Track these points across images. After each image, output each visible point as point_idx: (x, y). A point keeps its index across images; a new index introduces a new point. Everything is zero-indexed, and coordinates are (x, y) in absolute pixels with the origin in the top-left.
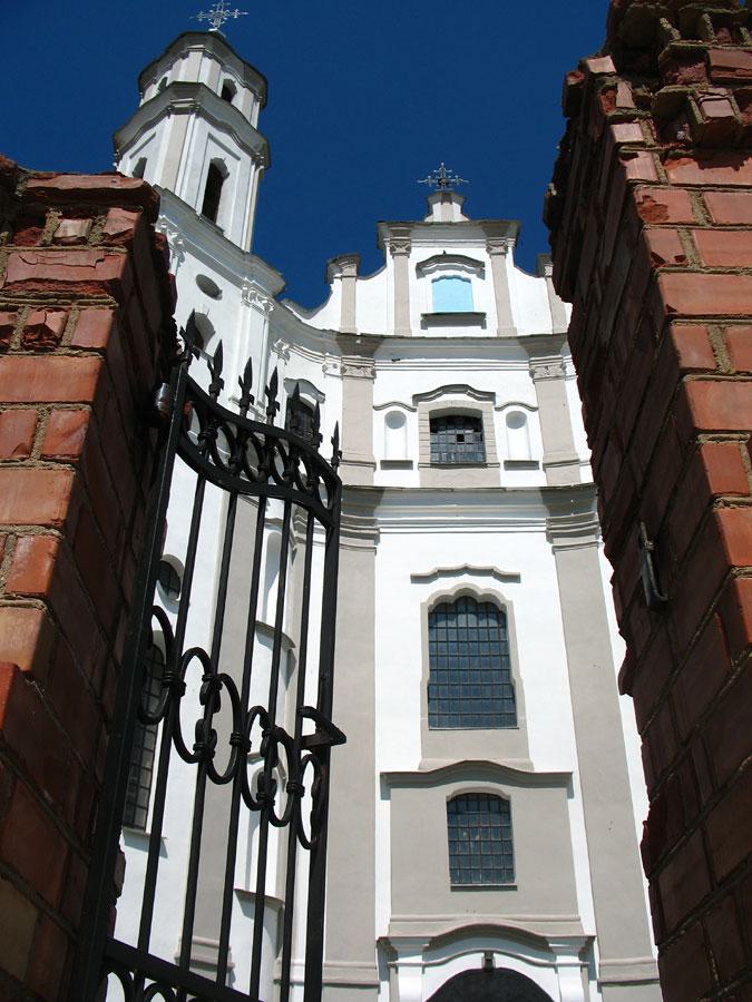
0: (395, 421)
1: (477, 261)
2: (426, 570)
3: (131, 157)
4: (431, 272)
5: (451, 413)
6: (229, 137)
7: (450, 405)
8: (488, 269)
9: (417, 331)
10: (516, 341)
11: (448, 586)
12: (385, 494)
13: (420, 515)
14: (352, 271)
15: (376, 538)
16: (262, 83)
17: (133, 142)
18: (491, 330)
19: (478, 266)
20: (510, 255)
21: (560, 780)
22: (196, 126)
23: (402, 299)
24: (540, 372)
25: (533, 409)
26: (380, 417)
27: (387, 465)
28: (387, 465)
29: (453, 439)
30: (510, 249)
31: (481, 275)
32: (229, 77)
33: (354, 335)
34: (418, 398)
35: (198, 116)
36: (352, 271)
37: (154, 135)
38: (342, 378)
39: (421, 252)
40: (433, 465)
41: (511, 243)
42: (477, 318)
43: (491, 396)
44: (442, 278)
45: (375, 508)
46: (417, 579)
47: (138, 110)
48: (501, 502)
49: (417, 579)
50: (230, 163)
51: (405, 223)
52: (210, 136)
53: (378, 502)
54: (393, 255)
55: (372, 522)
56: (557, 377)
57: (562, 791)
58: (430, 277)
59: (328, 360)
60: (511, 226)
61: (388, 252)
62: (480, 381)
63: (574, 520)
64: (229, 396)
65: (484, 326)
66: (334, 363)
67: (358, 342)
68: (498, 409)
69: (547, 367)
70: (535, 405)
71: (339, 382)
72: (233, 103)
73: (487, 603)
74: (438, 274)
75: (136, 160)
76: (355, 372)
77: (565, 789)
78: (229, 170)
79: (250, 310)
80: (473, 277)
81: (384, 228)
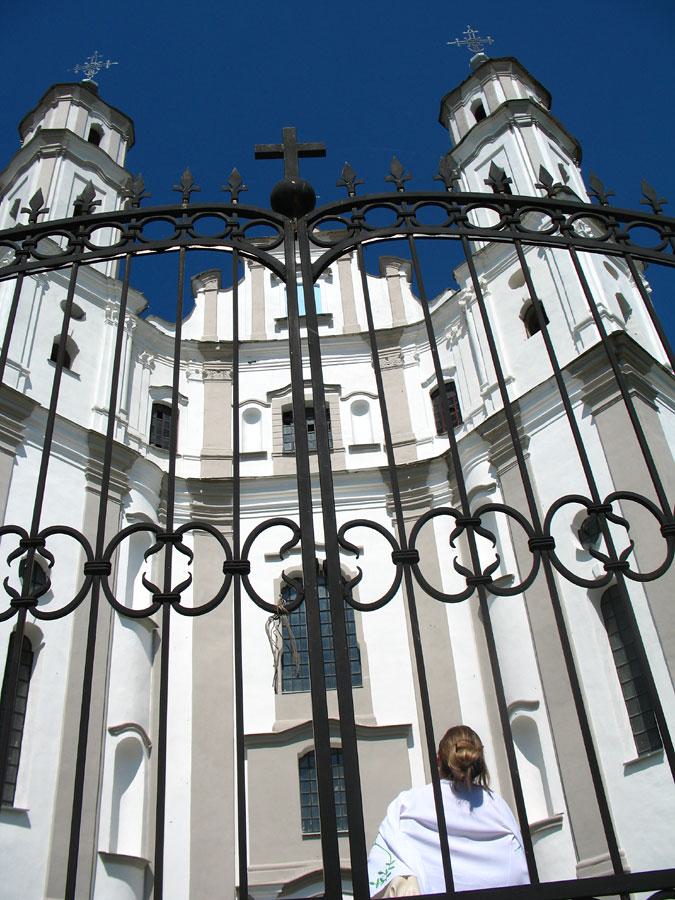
10: (359, 337)
13: (268, 500)
14: (214, 285)
16: (128, 124)
21: (402, 731)
33: (214, 342)
35: (64, 158)
37: (26, 179)
38: (204, 381)
52: (77, 176)
54: (251, 268)
56: (396, 367)
57: (403, 741)
67: (218, 348)
68: (343, 400)
71: (201, 385)
76: (217, 376)
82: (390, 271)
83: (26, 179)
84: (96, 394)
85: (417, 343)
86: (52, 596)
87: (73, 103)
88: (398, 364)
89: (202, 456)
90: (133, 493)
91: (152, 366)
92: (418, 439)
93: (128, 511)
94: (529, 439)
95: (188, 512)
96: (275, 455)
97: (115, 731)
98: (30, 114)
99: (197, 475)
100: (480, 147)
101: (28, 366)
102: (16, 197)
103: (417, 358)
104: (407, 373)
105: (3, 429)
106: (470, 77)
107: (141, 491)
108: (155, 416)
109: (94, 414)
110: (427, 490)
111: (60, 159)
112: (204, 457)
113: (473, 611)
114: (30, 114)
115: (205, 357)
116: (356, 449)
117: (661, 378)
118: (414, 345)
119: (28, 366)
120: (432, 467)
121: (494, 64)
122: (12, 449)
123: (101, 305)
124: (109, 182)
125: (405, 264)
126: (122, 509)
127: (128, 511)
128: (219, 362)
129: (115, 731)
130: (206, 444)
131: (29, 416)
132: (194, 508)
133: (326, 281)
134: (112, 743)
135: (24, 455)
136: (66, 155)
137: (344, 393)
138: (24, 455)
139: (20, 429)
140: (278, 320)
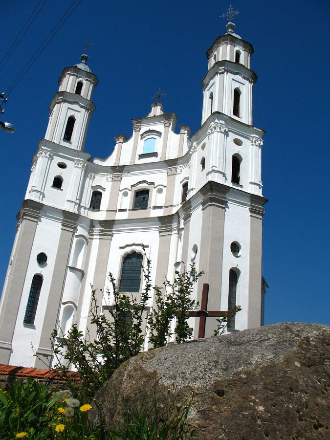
0: (126, 194)
2: (123, 245)
4: (145, 137)
7: (141, 188)
8: (163, 135)
9: (138, 162)
11: (128, 250)
13: (125, 227)
14: (121, 140)
15: (112, 236)
17: (208, 84)
19: (159, 134)
20: (171, 126)
22: (228, 77)
25: (165, 187)
26: (121, 193)
27: (121, 210)
28: (121, 210)
29: (142, 199)
31: (160, 136)
34: (132, 186)
36: (121, 140)
37: (214, 83)
38: (112, 181)
39: (144, 129)
40: (132, 210)
41: (172, 121)
42: (155, 154)
43: (153, 184)
44: (148, 139)
46: (121, 248)
47: (208, 72)
49: (121, 248)
51: (140, 119)
53: (114, 224)
59: (108, 176)
63: (167, 227)
64: (249, 182)
65: (157, 156)
66: (110, 176)
70: (165, 185)
71: (111, 183)
72: (240, 63)
73: (127, 255)
74: (147, 137)
76: (116, 179)
79: (254, 147)
80: (157, 137)
81: (134, 122)
82: (182, 131)
84: (68, 196)
86: (47, 265)
87: (70, 75)
89: (107, 211)
90: (79, 228)
91: (94, 177)
93: (76, 234)
97: (64, 304)
98: (60, 78)
100: (210, 80)
101: (44, 191)
102: (211, 90)
103: (181, 171)
104: (177, 176)
106: (214, 44)
107: (82, 227)
108: (94, 196)
109: (66, 202)
110: (171, 226)
113: (86, 278)
114: (60, 78)
116: (155, 208)
117: (120, 224)
118: (181, 165)
119: (44, 191)
120: (174, 217)
121: (221, 38)
122: (36, 220)
124: (82, 107)
127: (76, 234)
128: (118, 173)
129: (64, 304)
131: (42, 208)
132: (100, 230)
134: (63, 307)
135: (41, 221)
136: (64, 101)
137: (156, 185)
138: (41, 221)
139: (39, 213)
140: (139, 155)
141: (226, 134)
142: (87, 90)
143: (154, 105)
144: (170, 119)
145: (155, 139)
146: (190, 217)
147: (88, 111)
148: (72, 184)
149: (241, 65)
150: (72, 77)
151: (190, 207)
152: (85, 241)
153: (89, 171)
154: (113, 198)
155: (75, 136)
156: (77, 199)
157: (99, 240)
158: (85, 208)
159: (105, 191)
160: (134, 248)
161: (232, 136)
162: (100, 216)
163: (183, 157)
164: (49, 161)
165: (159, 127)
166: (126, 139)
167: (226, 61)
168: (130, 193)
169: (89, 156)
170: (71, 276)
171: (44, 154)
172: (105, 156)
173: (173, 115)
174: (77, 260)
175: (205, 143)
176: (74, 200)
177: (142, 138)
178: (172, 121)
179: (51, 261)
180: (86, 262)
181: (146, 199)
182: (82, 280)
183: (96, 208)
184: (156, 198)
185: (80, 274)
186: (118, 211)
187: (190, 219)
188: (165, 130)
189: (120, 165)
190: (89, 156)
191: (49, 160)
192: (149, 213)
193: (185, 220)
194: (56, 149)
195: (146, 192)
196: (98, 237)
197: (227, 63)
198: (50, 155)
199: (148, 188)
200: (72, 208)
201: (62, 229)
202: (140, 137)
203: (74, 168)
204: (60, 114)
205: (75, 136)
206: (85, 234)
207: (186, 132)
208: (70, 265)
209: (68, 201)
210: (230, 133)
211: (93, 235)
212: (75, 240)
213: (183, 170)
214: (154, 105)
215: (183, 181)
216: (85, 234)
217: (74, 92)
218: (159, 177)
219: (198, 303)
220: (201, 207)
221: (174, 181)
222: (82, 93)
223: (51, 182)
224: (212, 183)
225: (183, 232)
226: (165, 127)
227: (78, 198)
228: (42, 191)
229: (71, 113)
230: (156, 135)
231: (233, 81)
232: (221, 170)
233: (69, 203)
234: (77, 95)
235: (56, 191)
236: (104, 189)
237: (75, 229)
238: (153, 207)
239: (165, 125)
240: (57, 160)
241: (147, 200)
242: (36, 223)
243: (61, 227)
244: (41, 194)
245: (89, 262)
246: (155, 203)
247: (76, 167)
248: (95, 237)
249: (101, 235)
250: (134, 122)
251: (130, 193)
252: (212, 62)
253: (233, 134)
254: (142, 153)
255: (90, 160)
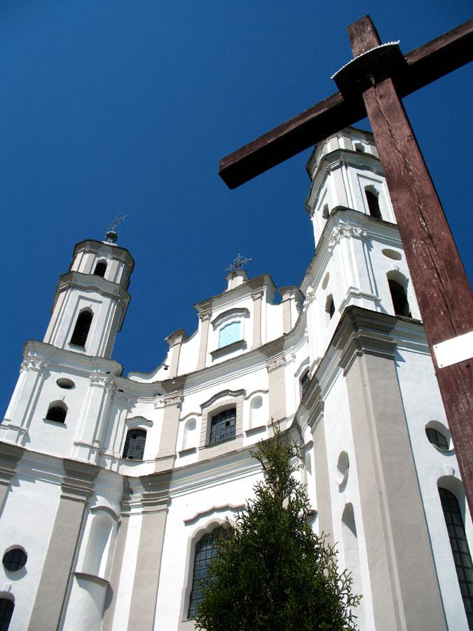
0: (191, 425)
1: (242, 309)
2: (191, 516)
3: (318, 210)
5: (223, 410)
6: (371, 172)
8: (251, 314)
9: (209, 363)
10: (258, 351)
11: (203, 523)
12: (173, 474)
15: (168, 502)
16: (125, 252)
17: (316, 201)
18: (251, 346)
19: (245, 312)
23: (258, 328)
24: (272, 366)
26: (183, 424)
30: (265, 294)
32: (358, 142)
33: (170, 380)
34: (203, 406)
35: (73, 288)
36: (179, 340)
37: (326, 190)
40: (206, 447)
41: (265, 289)
43: (242, 392)
45: (169, 483)
46: (188, 523)
48: (238, 459)
49: (188, 523)
50: (377, 187)
52: (358, 175)
53: (170, 479)
55: (167, 493)
58: (219, 328)
60: (265, 278)
61: (200, 320)
62: (233, 385)
65: (245, 347)
67: (174, 383)
69: (275, 362)
74: (224, 324)
75: (322, 209)
77: (440, 367)
78: (378, 191)
80: (242, 319)
81: (198, 307)
82: (285, 297)
83: (326, 190)
85: (294, 345)
86: (25, 573)
88: (282, 363)
89: (156, 459)
92: (288, 416)
94: (324, 403)
95: (139, 500)
96: (201, 449)
99: (152, 472)
102: (324, 203)
105: (2, 470)
111: (344, 168)
112: (158, 459)
115: (167, 390)
123: (86, 375)
125: (294, 290)
126: (87, 504)
130: (161, 450)
131: (20, 458)
133: (245, 317)
136: (73, 287)
138: (18, 485)
141: (366, 241)
142: (114, 271)
143: (230, 275)
144: (262, 285)
145: (239, 322)
146: (323, 409)
147: (117, 301)
148: (84, 415)
149: (368, 155)
150: (87, 256)
151: (319, 390)
152: (115, 520)
153: (120, 397)
154: (169, 434)
155: (91, 339)
156: (94, 441)
157: (141, 517)
158: (113, 458)
159: (151, 426)
160: (220, 517)
161: (378, 247)
162: (145, 469)
163: (293, 331)
164: (40, 378)
165: (246, 302)
166: (187, 338)
167: (340, 150)
168: (199, 420)
169: (118, 367)
170: (79, 596)
171: (30, 365)
172: (150, 367)
173: (267, 279)
174: (99, 567)
175: (328, 273)
176: (89, 442)
177: (215, 328)
178: (265, 289)
179: (35, 564)
180: (116, 565)
181: (232, 423)
182: (103, 614)
183: (137, 458)
184: (248, 417)
185: (102, 590)
186: (178, 455)
187: (322, 413)
188: (255, 305)
189: (179, 375)
190: (118, 367)
191: (39, 375)
192: (242, 443)
193: (311, 425)
194: (53, 359)
195: (230, 412)
196: (141, 510)
197: (342, 153)
198: (42, 366)
199: (233, 402)
200: (81, 456)
201: (62, 497)
202: (211, 326)
203: (89, 387)
204: (67, 306)
205: (91, 339)
206: (114, 507)
207: (293, 296)
208: (79, 569)
209: (77, 444)
210: (374, 243)
211: (129, 509)
212: (91, 517)
213: (296, 354)
214: (230, 275)
215: (299, 371)
216: (114, 507)
217: (92, 273)
218: (254, 379)
219: (377, 136)
220: (342, 371)
221: (282, 377)
222: (106, 276)
223: (42, 411)
224: (354, 312)
225: (311, 452)
226: (254, 300)
227: (97, 439)
228: (24, 427)
229: (83, 305)
230: (240, 316)
231: (361, 179)
232: (369, 293)
233: (79, 448)
234: (98, 278)
235: (53, 428)
236: (150, 423)
237: (91, 495)
238: (247, 432)
239: (253, 297)
240: (56, 376)
241: (234, 426)
242: (6, 488)
243: (61, 493)
244: (20, 434)
245: (120, 568)
246: (250, 423)
247: (92, 385)
248: (133, 511)
249: (144, 505)
250: (198, 307)
251: (199, 420)
252: (318, 221)
253: (375, 357)
254: (217, 348)
255: (123, 374)
